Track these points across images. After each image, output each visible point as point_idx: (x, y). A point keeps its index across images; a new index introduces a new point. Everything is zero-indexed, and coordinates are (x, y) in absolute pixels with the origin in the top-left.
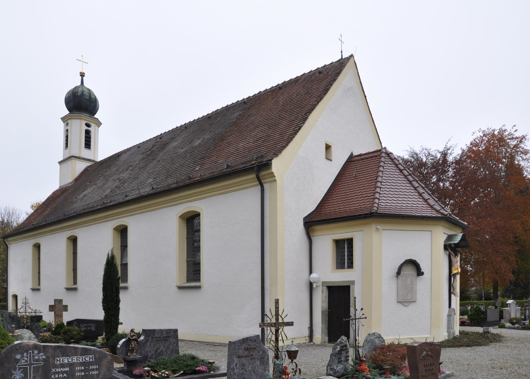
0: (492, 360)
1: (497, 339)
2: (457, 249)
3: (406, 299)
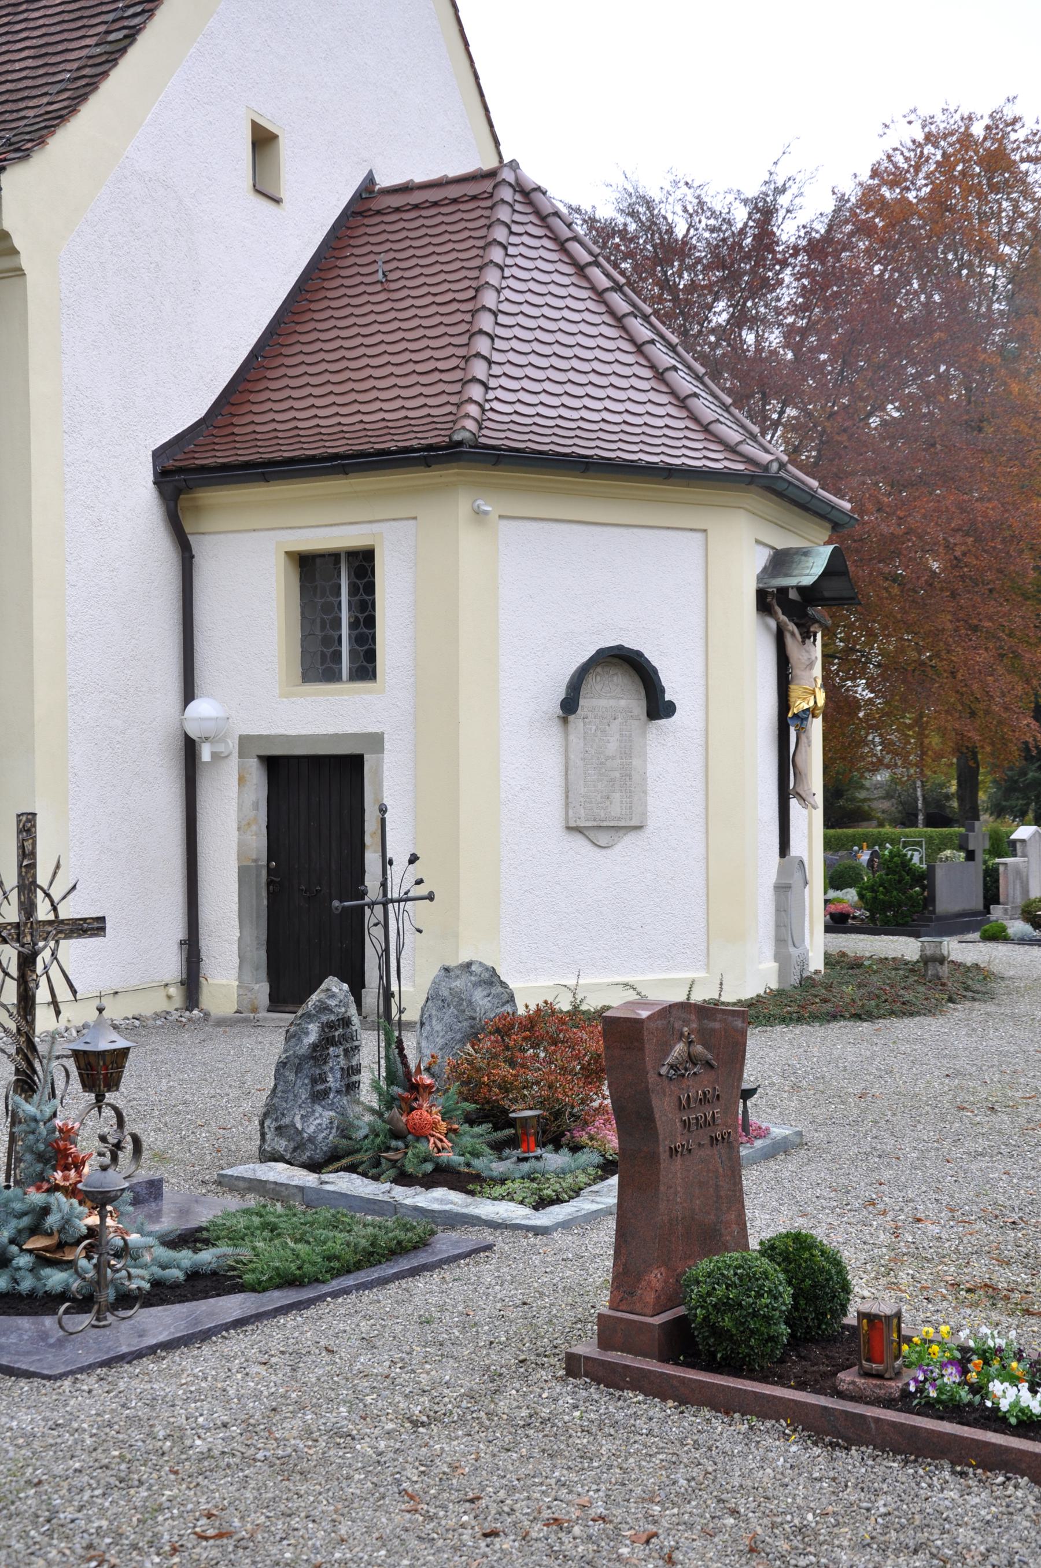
0: (958, 1073)
1: (973, 985)
2: (811, 611)
3: (601, 821)
